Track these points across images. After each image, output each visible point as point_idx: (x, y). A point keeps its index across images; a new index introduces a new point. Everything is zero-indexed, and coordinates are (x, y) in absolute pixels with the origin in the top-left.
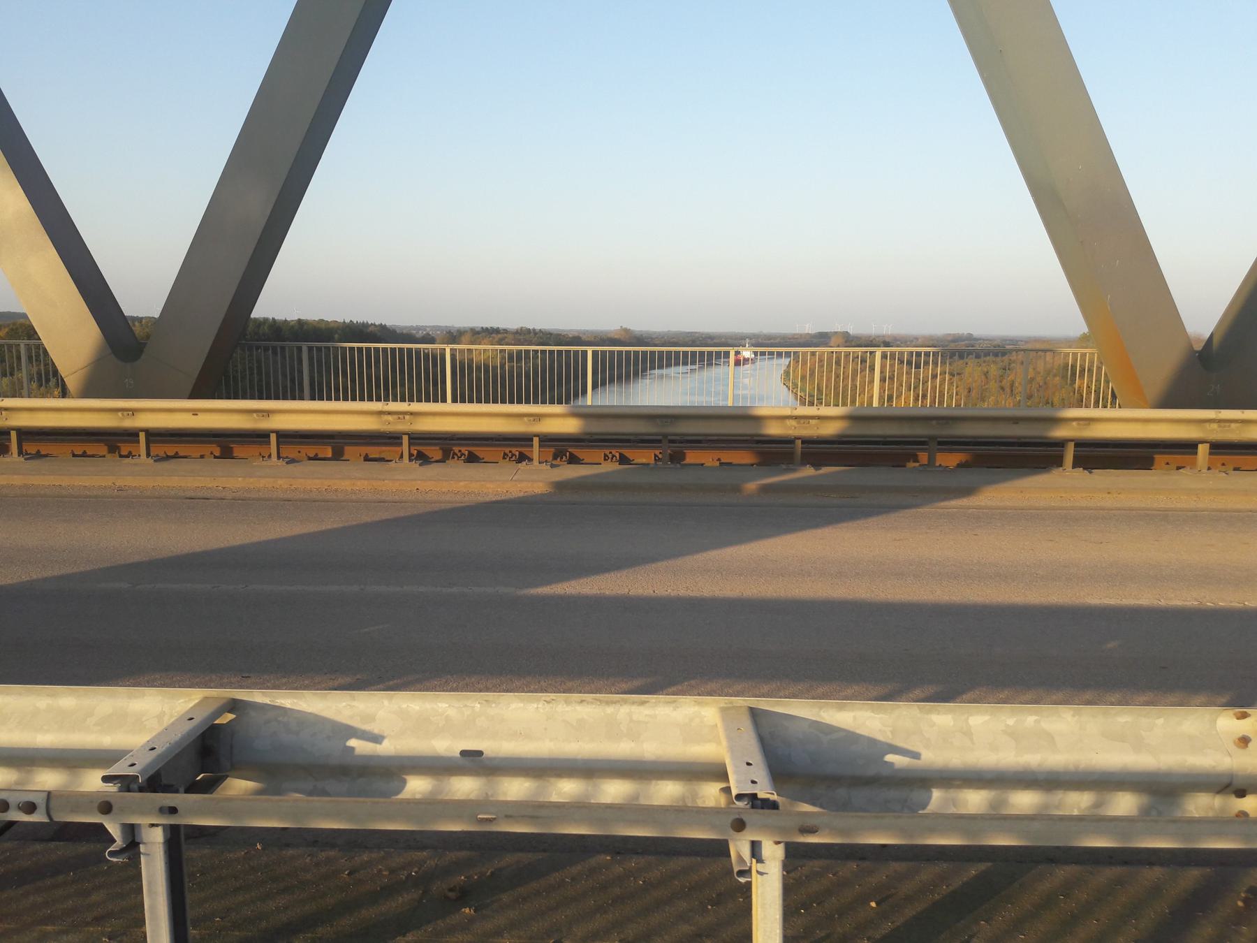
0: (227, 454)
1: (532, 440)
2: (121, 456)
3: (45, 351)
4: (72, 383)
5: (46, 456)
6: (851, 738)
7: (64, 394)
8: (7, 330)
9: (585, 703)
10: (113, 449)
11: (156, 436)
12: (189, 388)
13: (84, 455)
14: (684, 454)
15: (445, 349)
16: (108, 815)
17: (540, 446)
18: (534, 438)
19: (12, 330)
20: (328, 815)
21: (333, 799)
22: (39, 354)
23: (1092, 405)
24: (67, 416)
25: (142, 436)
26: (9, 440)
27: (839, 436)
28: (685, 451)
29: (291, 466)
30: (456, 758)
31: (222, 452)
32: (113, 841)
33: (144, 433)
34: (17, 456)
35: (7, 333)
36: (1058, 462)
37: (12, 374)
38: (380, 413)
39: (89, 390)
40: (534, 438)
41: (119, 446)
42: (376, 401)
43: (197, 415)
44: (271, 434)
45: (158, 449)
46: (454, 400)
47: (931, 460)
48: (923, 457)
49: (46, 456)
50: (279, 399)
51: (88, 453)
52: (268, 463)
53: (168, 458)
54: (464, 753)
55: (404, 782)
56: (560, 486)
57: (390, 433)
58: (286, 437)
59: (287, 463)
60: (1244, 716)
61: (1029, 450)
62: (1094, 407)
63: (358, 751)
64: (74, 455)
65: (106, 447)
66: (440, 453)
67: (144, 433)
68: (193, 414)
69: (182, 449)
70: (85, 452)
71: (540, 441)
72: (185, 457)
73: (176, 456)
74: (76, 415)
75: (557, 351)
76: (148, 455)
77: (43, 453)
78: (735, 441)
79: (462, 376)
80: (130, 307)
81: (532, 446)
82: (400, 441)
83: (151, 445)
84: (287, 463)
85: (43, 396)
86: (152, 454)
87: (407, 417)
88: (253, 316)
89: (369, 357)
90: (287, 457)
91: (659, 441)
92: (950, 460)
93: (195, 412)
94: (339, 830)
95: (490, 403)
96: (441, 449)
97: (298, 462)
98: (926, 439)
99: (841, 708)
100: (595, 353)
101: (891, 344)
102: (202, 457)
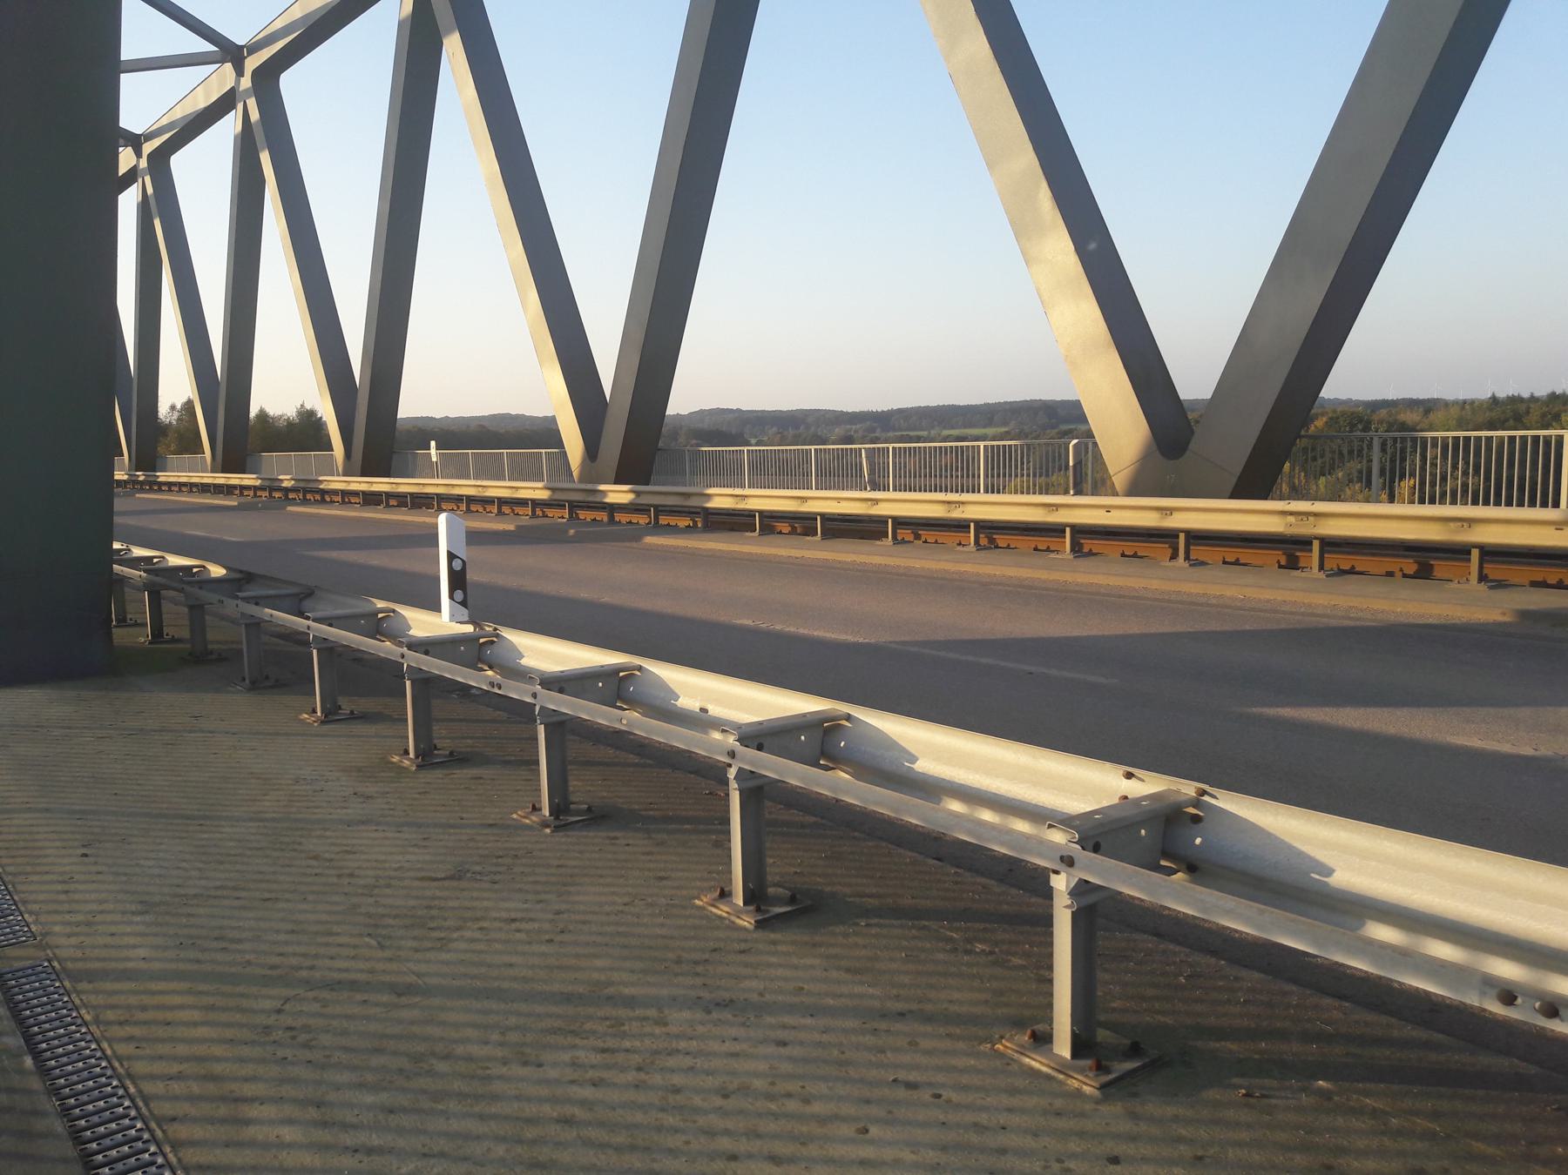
0: (1424, 573)
1: (1469, 553)
4: (1119, 479)
6: (890, 744)
7: (1115, 494)
8: (1325, 419)
12: (1230, 487)
13: (1237, 563)
15: (1563, 436)
16: (1509, 1007)
18: (1473, 550)
19: (1331, 419)
20: (1294, 934)
21: (1310, 921)
23: (1550, 504)
24: (844, 504)
25: (1475, 553)
27: (631, 504)
31: (1288, 561)
33: (1183, 534)
34: (1476, 582)
35: (1326, 422)
37: (1047, 476)
38: (1284, 513)
39: (1135, 489)
40: (1314, 541)
41: (1432, 565)
42: (1483, 505)
43: (1562, 529)
44: (1314, 541)
45: (1333, 560)
46: (895, 490)
51: (1052, 549)
53: (1342, 572)
55: (1363, 925)
56: (1525, 615)
57: (1292, 536)
59: (1327, 576)
60: (1129, 776)
61: (853, 526)
62: (1027, 494)
64: (1225, 562)
66: (790, 528)
67: (1183, 534)
68: (1557, 529)
69: (1361, 562)
73: (1352, 571)
74: (1394, 524)
75: (1509, 437)
76: (1321, 568)
77: (1139, 554)
78: (589, 507)
81: (1469, 560)
82: (1309, 547)
83: (1192, 547)
84: (1190, 565)
85: (1367, 501)
86: (1327, 566)
87: (1311, 518)
91: (605, 508)
92: (684, 522)
93: (839, 500)
94: (967, 842)
95: (1435, 503)
98: (648, 508)
101: (1418, 428)
102: (1390, 574)
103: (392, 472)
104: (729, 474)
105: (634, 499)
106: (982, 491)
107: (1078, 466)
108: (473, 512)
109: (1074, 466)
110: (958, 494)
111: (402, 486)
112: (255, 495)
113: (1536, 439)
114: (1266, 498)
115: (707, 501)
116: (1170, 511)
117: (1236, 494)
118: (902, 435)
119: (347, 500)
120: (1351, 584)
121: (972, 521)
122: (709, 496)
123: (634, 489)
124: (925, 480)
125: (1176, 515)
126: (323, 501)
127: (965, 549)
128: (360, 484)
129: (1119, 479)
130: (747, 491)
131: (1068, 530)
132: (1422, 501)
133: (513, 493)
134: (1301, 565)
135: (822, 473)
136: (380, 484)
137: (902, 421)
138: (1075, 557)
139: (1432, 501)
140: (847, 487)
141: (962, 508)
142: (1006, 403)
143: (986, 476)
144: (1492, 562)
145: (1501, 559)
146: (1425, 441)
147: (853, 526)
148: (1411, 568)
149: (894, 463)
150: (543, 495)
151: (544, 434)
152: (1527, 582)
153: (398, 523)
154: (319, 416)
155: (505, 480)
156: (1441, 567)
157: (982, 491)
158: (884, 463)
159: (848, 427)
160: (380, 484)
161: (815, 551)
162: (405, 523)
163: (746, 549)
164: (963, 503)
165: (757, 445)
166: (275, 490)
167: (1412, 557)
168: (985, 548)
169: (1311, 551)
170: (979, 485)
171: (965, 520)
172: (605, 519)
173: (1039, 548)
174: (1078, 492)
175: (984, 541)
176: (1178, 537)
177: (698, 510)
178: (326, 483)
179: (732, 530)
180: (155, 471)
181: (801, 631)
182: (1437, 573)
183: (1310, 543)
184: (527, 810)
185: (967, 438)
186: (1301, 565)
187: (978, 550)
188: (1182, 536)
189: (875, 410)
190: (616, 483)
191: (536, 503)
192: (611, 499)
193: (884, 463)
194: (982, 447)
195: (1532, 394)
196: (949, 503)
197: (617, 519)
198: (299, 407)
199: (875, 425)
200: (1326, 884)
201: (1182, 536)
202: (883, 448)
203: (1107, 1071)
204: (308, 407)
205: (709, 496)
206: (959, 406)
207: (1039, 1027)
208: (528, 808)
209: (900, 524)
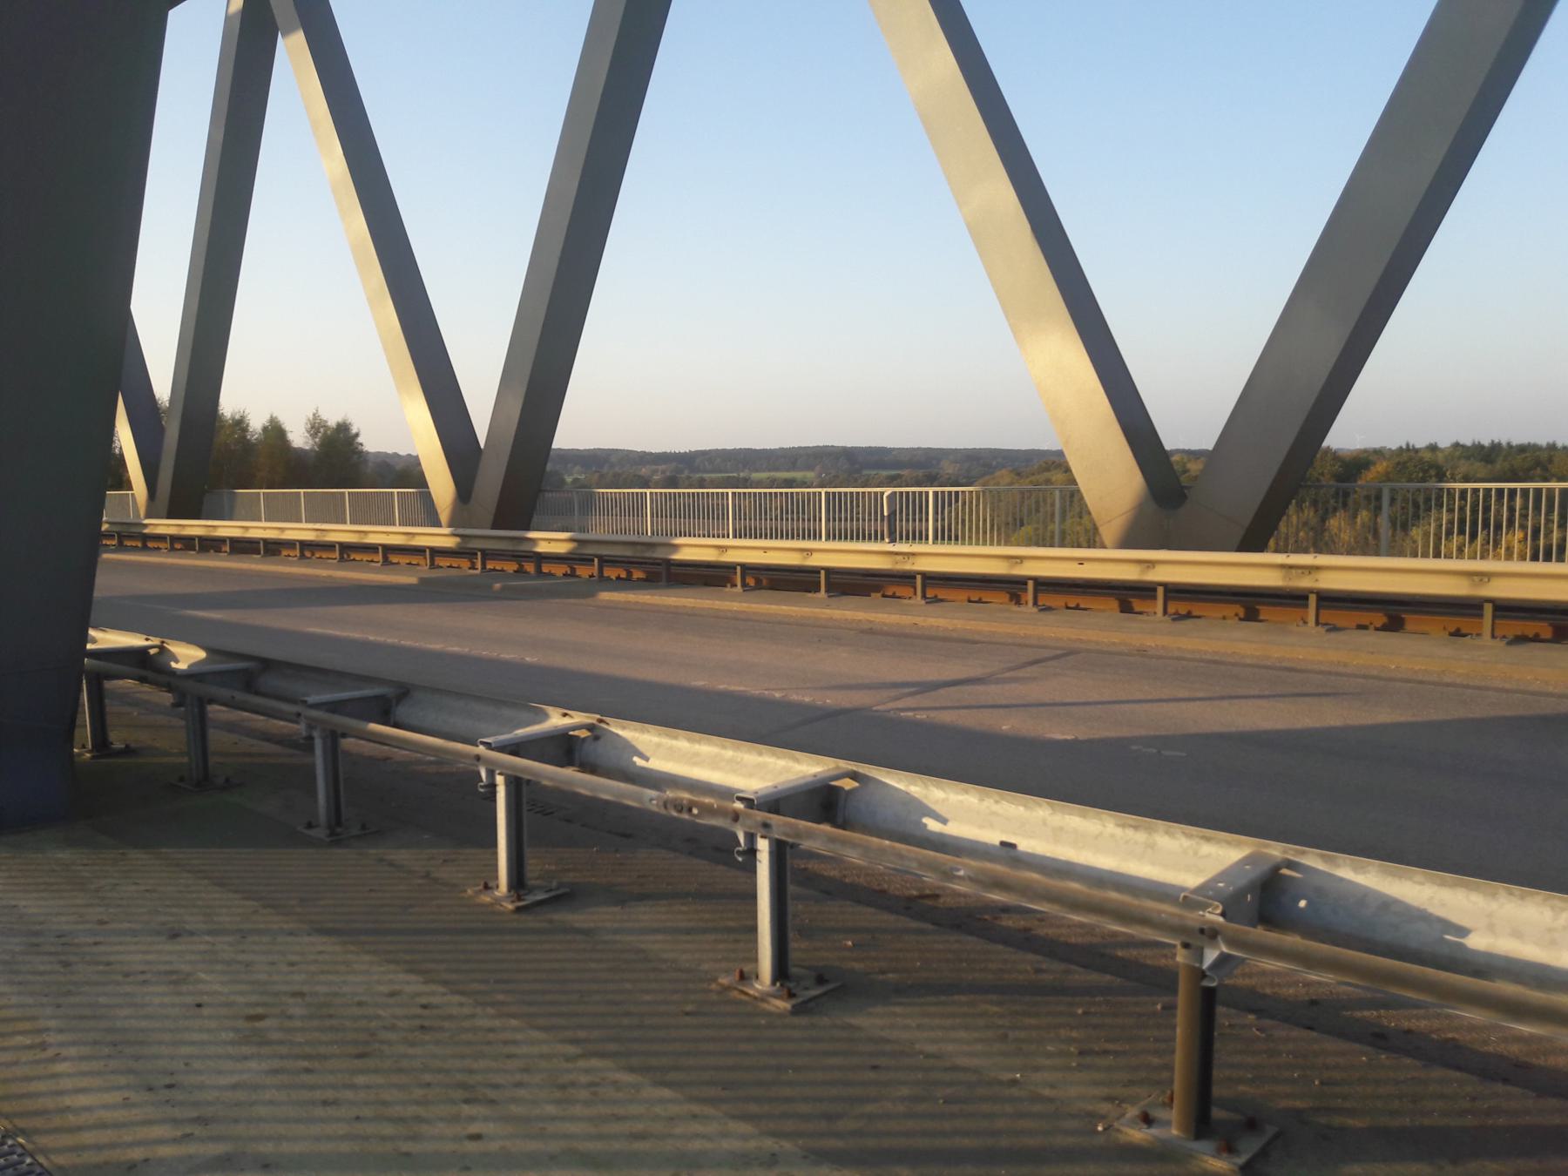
0: (1251, 616)
1: (1026, 584)
2: (884, 596)
3: (1082, 498)
4: (1109, 532)
5: (942, 600)
7: (1103, 547)
9: (567, 717)
10: (1126, 608)
11: (1177, 592)
13: (1077, 608)
14: (1258, 611)
17: (1494, 617)
22: (1073, 496)
23: (1515, 556)
24: (391, 536)
25: (1031, 584)
26: (1026, 590)
27: (570, 553)
28: (1403, 616)
29: (1333, 635)
30: (994, 846)
32: (740, 845)
36: (815, 588)
38: (1282, 566)
46: (735, 537)
47: (349, 556)
48: (285, 553)
49: (942, 600)
50: (1406, 556)
52: (734, 590)
54: (1003, 844)
58: (1330, 600)
63: (638, 764)
65: (1008, 596)
70: (1078, 605)
71: (922, 578)
72: (1199, 617)
74: (1397, 578)
75: (1509, 489)
76: (1165, 612)
79: (723, 514)
80: (1172, 438)
82: (1153, 593)
86: (1040, 603)
88: (1325, 444)
89: (792, 497)
90: (1326, 624)
91: (531, 557)
93: (765, 550)
95: (1440, 557)
96: (1551, 625)
97: (1054, 609)
98: (592, 557)
99: (642, 731)
100: (827, 494)
102: (1224, 618)
103: (532, 525)
104: (707, 519)
105: (575, 549)
106: (731, 536)
107: (892, 516)
108: (150, 549)
109: (889, 516)
110: (909, 545)
111: (333, 534)
112: (433, 566)
113: (1538, 492)
114: (1262, 551)
115: (144, 529)
116: (1151, 564)
117: (1243, 547)
118: (729, 477)
119: (345, 556)
120: (1049, 617)
121: (1312, 592)
122: (676, 547)
123: (456, 532)
124: (792, 524)
125: (251, 531)
126: (145, 548)
127: (911, 602)
128: (165, 526)
129: (1109, 532)
130: (730, 542)
131: (739, 568)
132: (1535, 558)
133: (805, 558)
134: (1261, 617)
135: (740, 515)
136: (194, 527)
137: (706, 463)
138: (829, 597)
139: (1548, 558)
140: (745, 535)
141: (912, 559)
142: (800, 448)
143: (828, 520)
144: (607, 566)
145: (1513, 614)
146: (1450, 492)
147: (711, 572)
148: (1380, 619)
149: (734, 505)
150: (450, 543)
151: (407, 473)
152: (1354, 625)
153: (242, 574)
154: (354, 431)
155: (345, 523)
156: (1412, 621)
157: (731, 536)
158: (723, 505)
159: (654, 467)
160: (194, 527)
161: (1058, 628)
162: (260, 575)
163: (254, 567)
164: (913, 554)
165: (994, 485)
166: (607, 561)
167: (565, 564)
168: (754, 589)
169: (1481, 616)
170: (927, 530)
171: (910, 571)
172: (140, 545)
173: (972, 599)
174: (893, 540)
175: (751, 582)
176: (915, 578)
177: (531, 554)
178: (152, 527)
179: (707, 584)
180: (528, 529)
181: (732, 688)
182: (1408, 627)
183: (1155, 590)
184: (477, 888)
185: (805, 483)
186: (1261, 617)
187: (744, 591)
188: (919, 577)
189: (677, 452)
190: (169, 517)
191: (436, 552)
192: (542, 548)
193: (723, 505)
194: (302, 494)
195: (1493, 441)
196: (1291, 567)
197: (606, 574)
198: (311, 417)
199: (681, 466)
200: (1462, 946)
201: (919, 577)
202: (722, 493)
203: (519, 899)
204: (332, 420)
205: (676, 547)
206: (755, 450)
207: (747, 968)
208: (478, 885)
209: (607, 561)
